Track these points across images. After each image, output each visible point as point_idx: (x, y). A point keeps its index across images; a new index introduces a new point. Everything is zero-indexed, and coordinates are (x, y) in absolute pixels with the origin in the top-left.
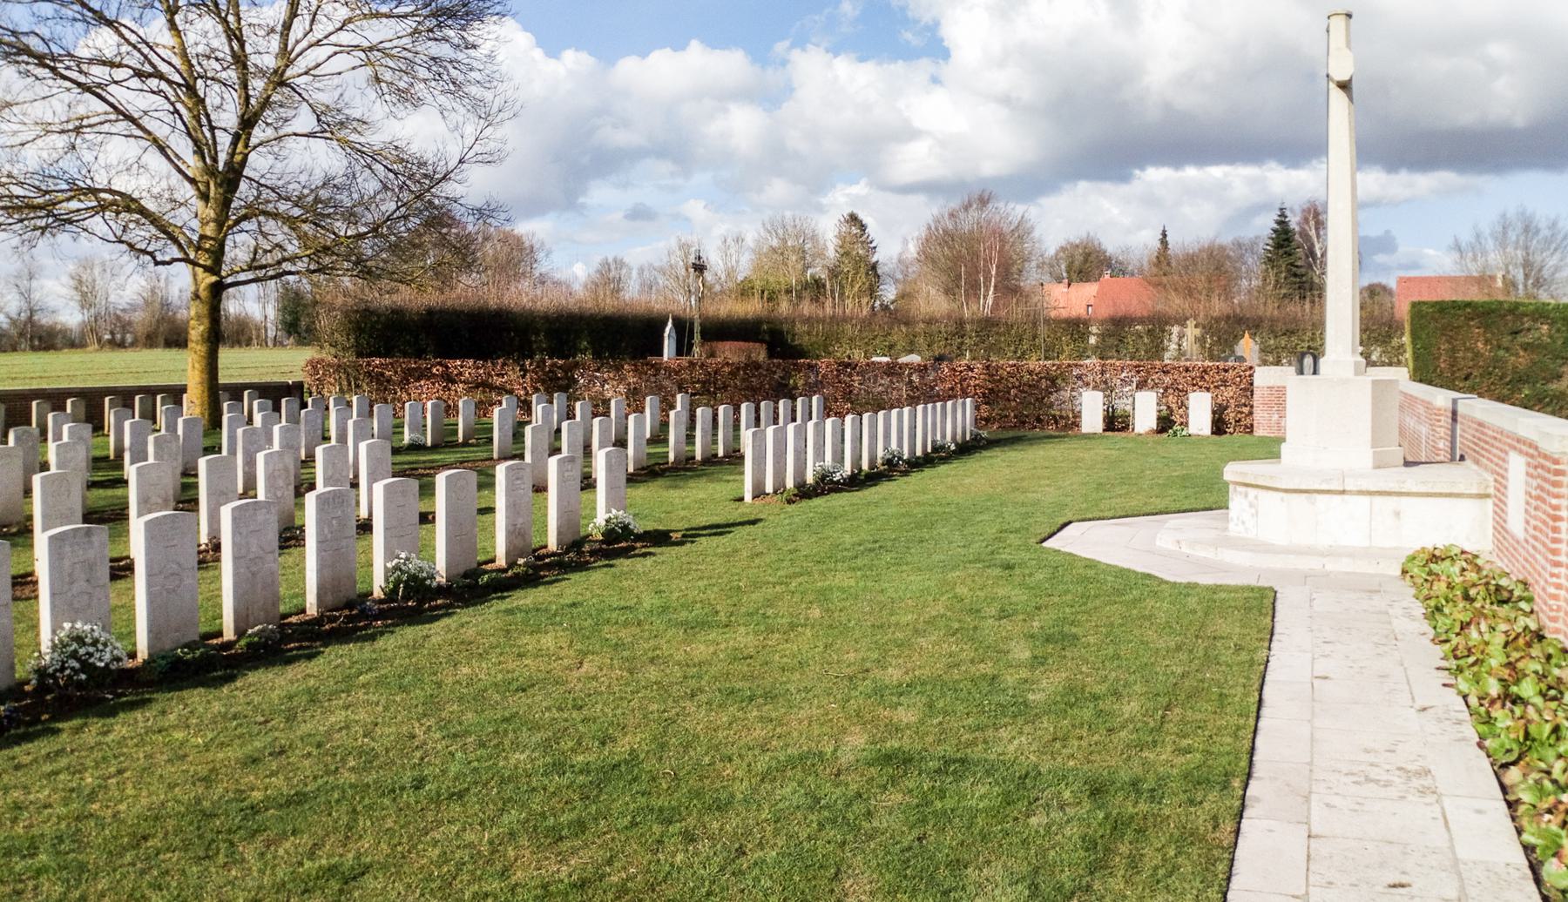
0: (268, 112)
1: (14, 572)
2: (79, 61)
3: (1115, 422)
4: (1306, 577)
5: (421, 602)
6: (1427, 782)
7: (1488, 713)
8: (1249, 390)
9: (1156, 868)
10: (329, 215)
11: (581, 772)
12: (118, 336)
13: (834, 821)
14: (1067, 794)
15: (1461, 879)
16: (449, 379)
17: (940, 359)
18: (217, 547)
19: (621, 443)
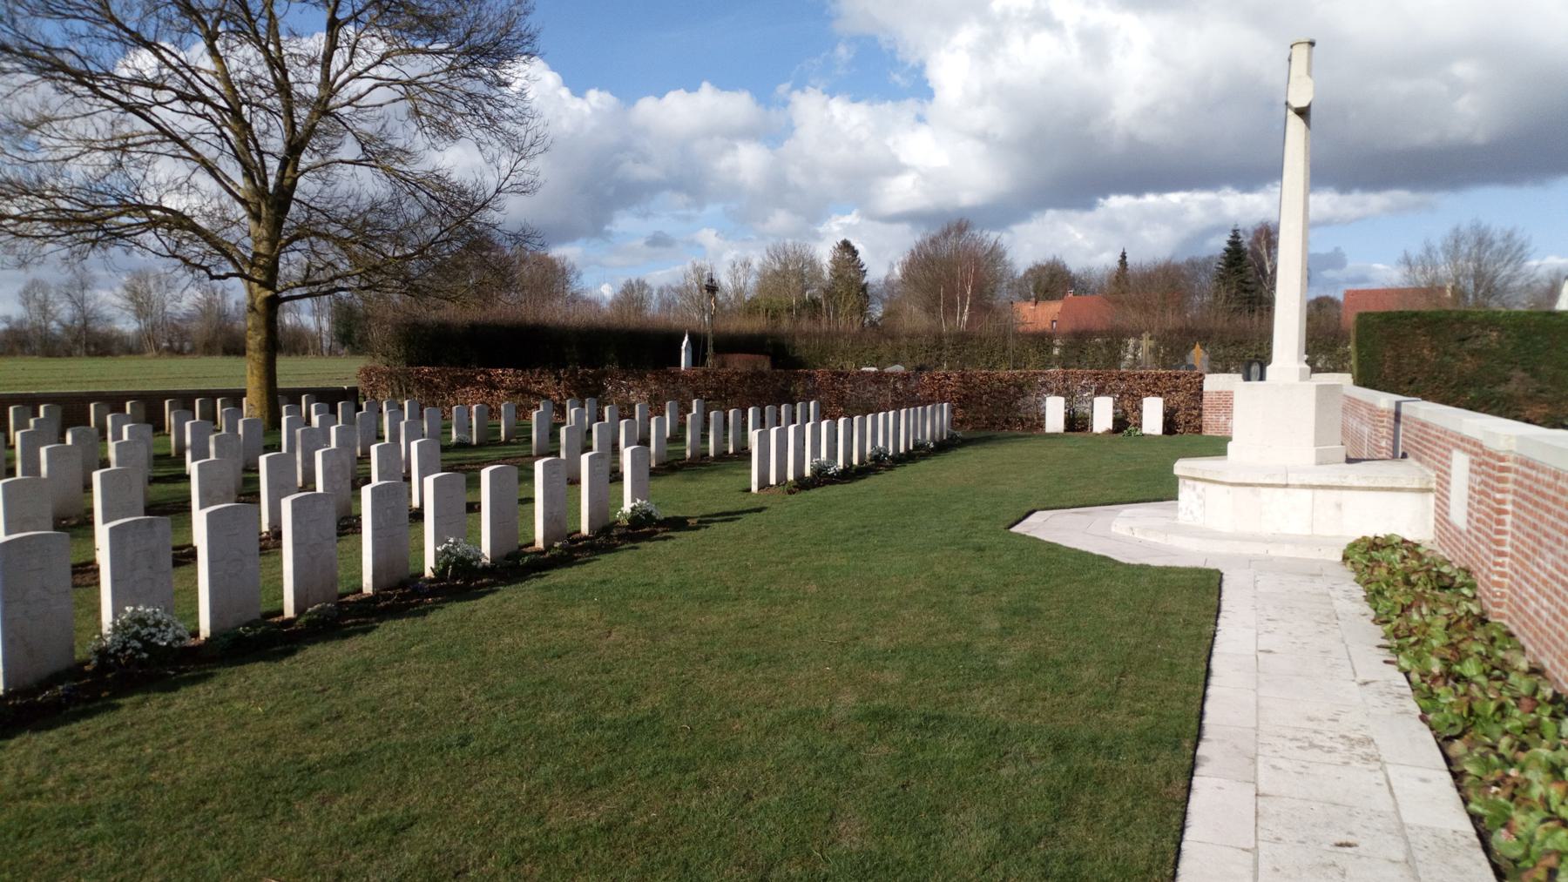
0: (313, 140)
1: (75, 560)
2: (120, 81)
3: (1077, 423)
4: (1250, 561)
5: (468, 581)
6: (1371, 750)
7: (1430, 689)
8: (1199, 393)
9: (1115, 818)
10: (377, 238)
11: (609, 728)
12: (177, 344)
13: (829, 770)
14: (1033, 749)
15: (1407, 842)
16: (492, 386)
17: (920, 369)
18: (277, 534)
19: (645, 442)
